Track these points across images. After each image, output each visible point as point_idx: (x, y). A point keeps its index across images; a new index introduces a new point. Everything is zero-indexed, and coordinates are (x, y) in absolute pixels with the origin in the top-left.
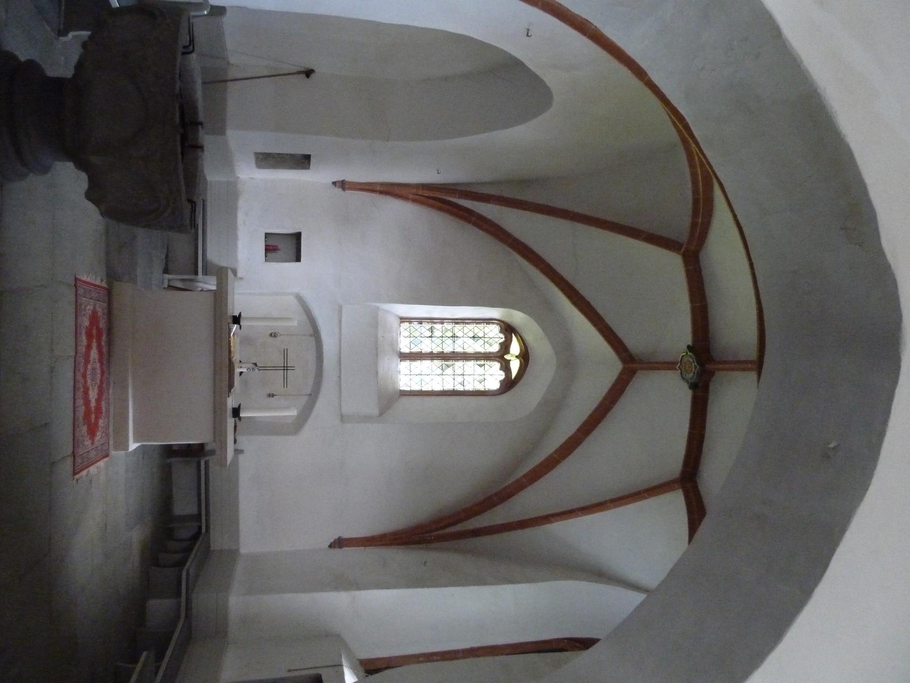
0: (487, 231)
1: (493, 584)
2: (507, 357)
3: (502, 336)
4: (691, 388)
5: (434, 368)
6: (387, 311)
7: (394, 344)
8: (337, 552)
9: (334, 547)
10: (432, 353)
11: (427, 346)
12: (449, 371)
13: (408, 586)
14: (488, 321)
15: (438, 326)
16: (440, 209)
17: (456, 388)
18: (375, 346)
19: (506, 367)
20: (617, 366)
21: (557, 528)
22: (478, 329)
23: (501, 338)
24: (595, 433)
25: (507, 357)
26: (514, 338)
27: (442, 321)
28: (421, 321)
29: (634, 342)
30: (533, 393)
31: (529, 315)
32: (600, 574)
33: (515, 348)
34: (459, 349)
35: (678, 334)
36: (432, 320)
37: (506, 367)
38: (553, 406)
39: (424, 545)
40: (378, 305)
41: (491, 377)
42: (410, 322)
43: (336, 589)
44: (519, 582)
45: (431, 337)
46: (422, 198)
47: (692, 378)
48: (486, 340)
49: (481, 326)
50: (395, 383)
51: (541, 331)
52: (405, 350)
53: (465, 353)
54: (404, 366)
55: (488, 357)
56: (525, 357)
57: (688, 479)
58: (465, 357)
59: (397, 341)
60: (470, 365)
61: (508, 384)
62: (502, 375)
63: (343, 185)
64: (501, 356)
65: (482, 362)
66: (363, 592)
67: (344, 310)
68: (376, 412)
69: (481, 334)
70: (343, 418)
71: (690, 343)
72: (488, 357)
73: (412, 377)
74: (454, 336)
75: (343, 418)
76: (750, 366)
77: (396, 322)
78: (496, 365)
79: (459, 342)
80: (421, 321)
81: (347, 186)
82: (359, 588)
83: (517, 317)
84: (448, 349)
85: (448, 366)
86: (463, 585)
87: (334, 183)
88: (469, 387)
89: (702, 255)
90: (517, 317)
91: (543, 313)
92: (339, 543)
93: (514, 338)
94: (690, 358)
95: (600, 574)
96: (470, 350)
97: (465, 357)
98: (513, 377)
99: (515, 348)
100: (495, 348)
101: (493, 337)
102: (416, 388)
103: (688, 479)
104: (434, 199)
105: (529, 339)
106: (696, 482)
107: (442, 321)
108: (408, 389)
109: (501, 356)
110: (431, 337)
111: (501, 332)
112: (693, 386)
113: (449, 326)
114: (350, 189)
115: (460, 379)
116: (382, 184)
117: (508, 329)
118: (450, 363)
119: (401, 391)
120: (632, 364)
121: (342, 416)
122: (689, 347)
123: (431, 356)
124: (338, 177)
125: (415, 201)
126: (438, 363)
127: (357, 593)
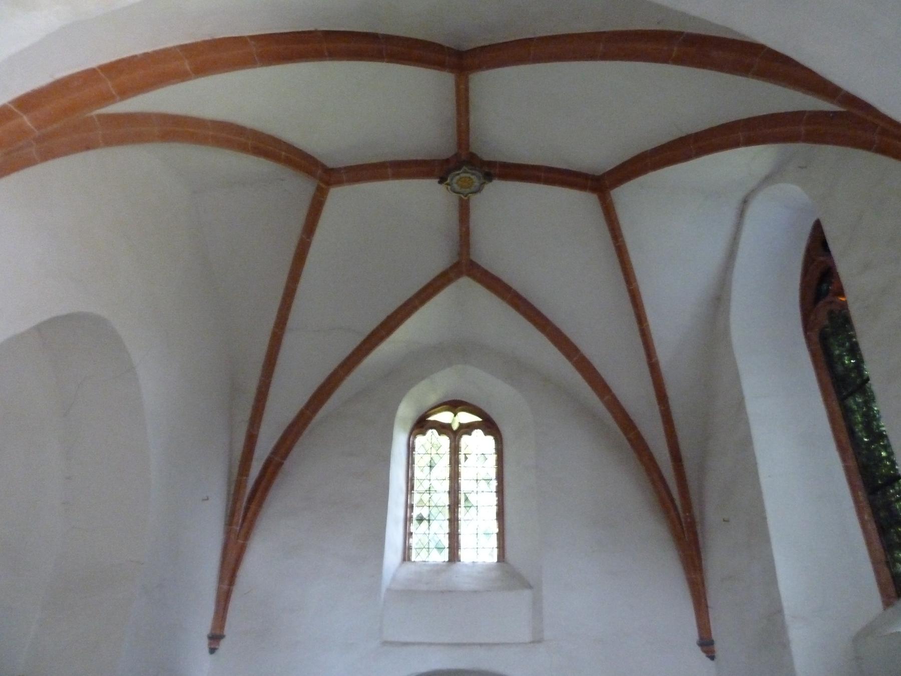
0: (294, 442)
1: (747, 423)
2: (455, 427)
3: (430, 432)
4: (490, 180)
5: (468, 516)
6: (394, 579)
7: (437, 570)
8: (719, 647)
9: (713, 651)
10: (450, 520)
11: (442, 527)
12: (472, 498)
13: (767, 540)
14: (411, 449)
15: (416, 513)
16: (260, 505)
17: (494, 489)
18: (436, 591)
19: (467, 429)
20: (465, 283)
21: (663, 355)
22: (420, 461)
23: (432, 433)
24: (544, 311)
25: (455, 427)
26: (431, 418)
27: (409, 507)
28: (408, 534)
29: (437, 260)
30: (499, 394)
31: (404, 395)
32: (718, 300)
33: (444, 417)
34: (446, 485)
35: (428, 198)
36: (408, 520)
37: (467, 429)
38: (515, 369)
39: (699, 528)
40: (384, 590)
41: (479, 447)
42: (410, 548)
43: (785, 645)
44: (741, 392)
45: (429, 521)
46: (245, 524)
47: (479, 178)
48: (434, 451)
49: (417, 458)
50: (489, 568)
51: (423, 382)
52: (445, 556)
53: (451, 478)
54: (466, 555)
55: (455, 450)
56: (454, 406)
57: (600, 184)
58: (455, 476)
59: (430, 565)
60: (465, 470)
61: (489, 426)
62: (478, 433)
63: (215, 638)
64: (455, 434)
65: (462, 457)
66: (785, 604)
67: (390, 639)
68: (527, 594)
69: (427, 459)
70: (537, 641)
71: (437, 180)
72: (455, 450)
73: (480, 546)
74: (429, 491)
75: (537, 641)
76: (462, 86)
77: (408, 565)
78: (465, 440)
79: (436, 485)
80: (408, 534)
81: (218, 632)
82: (780, 611)
83: (406, 412)
84: (445, 500)
85: (466, 499)
86: (755, 464)
87: (212, 651)
88: (493, 473)
89: (330, 164)
90: (406, 412)
91: (401, 377)
92: (707, 645)
93: (431, 418)
94: (455, 179)
95: (718, 300)
96: (447, 474)
97: (455, 476)
98: (479, 419)
99: (444, 417)
100: (445, 441)
101: (432, 444)
102: (494, 542)
103: (600, 184)
104: (247, 509)
105: (433, 399)
106: (604, 174)
107: (409, 507)
108: (496, 551)
109: (455, 434)
110: (429, 521)
111: (424, 433)
112: (489, 177)
113: (416, 497)
114: (222, 627)
115: (483, 484)
116: (221, 580)
117: (421, 425)
118: (462, 498)
119: (498, 561)
120: (464, 266)
121: (533, 642)
122: (440, 182)
123: (454, 521)
124: (204, 643)
125: (247, 536)
126: (462, 510)
127: (787, 612)
